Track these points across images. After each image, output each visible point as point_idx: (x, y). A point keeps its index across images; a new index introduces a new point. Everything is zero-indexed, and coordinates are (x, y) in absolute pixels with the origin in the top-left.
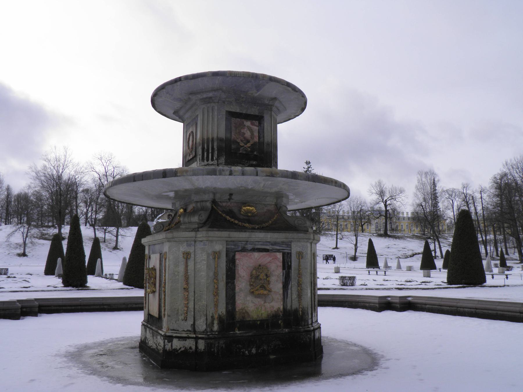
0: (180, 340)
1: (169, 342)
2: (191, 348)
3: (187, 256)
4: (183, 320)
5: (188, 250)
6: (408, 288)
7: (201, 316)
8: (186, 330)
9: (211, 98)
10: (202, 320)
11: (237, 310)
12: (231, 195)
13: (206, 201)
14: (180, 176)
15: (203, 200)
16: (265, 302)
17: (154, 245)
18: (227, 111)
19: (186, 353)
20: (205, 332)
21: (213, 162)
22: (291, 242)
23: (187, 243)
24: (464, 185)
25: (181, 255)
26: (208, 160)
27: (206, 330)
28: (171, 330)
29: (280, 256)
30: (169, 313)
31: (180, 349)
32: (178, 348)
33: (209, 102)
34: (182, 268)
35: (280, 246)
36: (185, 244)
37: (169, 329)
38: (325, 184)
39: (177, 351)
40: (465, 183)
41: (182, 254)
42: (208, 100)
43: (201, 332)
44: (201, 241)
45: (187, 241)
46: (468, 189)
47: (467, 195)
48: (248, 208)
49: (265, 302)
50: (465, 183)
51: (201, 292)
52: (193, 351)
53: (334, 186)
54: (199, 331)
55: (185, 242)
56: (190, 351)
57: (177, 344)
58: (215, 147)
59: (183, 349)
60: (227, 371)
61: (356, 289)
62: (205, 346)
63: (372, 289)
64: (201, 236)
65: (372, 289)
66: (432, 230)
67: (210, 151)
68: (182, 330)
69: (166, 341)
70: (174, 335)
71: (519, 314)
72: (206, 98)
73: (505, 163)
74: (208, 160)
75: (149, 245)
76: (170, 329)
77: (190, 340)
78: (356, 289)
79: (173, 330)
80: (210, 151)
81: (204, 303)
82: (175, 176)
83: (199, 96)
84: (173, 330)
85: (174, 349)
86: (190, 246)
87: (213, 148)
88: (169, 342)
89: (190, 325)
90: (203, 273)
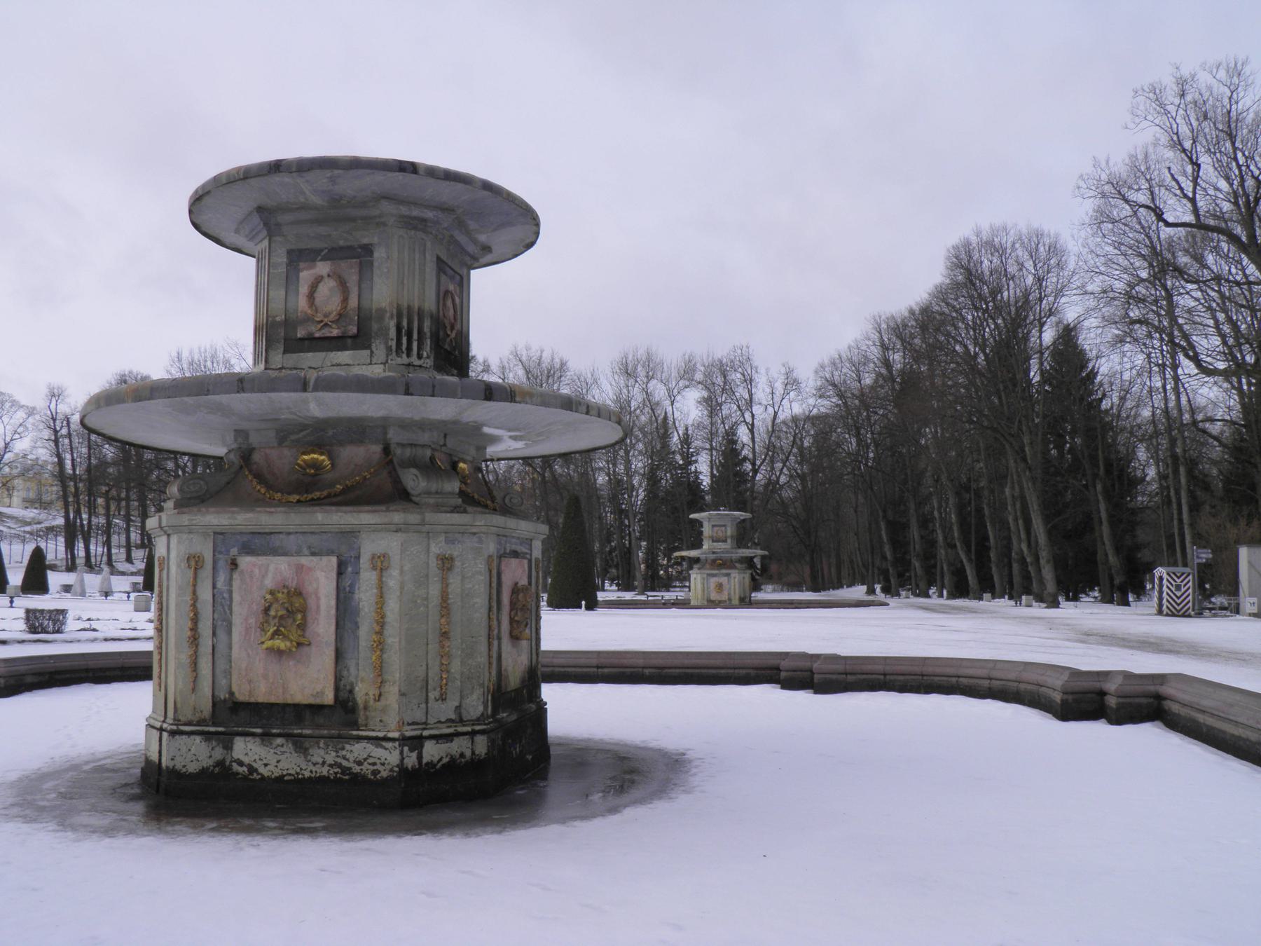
0: (440, 741)
1: (411, 750)
2: (462, 755)
3: (446, 563)
4: (437, 700)
5: (449, 552)
7: (473, 688)
8: (443, 720)
9: (424, 220)
10: (475, 696)
13: (423, 446)
14: (520, 403)
15: (415, 443)
17: (289, 534)
19: (453, 767)
20: (482, 718)
21: (422, 360)
22: (531, 540)
23: (446, 537)
24: (54, 388)
25: (433, 563)
26: (409, 355)
27: (482, 714)
28: (409, 724)
30: (402, 689)
31: (441, 759)
32: (435, 760)
33: (415, 228)
34: (434, 590)
36: (442, 538)
37: (403, 723)
39: (435, 765)
40: (55, 386)
41: (435, 560)
42: (414, 224)
43: (472, 720)
44: (474, 534)
45: (446, 533)
46: (63, 400)
47: (56, 413)
48: (315, 456)
50: (55, 386)
51: (474, 639)
52: (467, 762)
54: (469, 718)
55: (443, 535)
56: (461, 762)
57: (432, 751)
58: (426, 329)
59: (445, 760)
60: (319, 821)
61: (79, 641)
62: (488, 746)
63: (119, 640)
64: (482, 523)
65: (119, 640)
67: (415, 336)
68: (436, 721)
69: (406, 749)
70: (426, 733)
71: (595, 670)
72: (415, 218)
73: (174, 354)
74: (409, 355)
76: (406, 723)
77: (461, 738)
78: (79, 641)
79: (413, 723)
80: (415, 336)
81: (479, 660)
82: (511, 402)
83: (404, 210)
84: (413, 723)
85: (427, 764)
86: (454, 544)
87: (420, 331)
88: (411, 750)
89: (453, 709)
90: (478, 600)
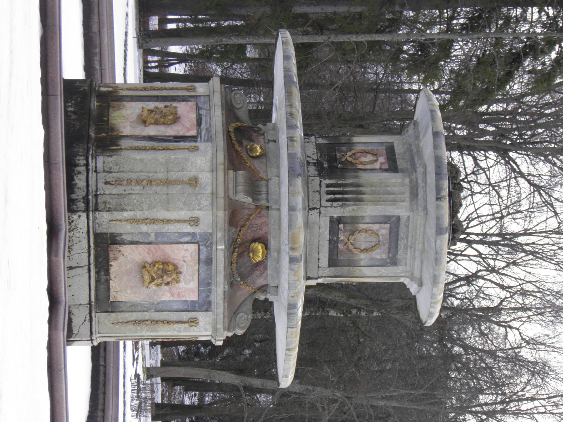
6: (108, 352)
11: (123, 103)
12: (275, 141)
16: (131, 122)
18: (393, 143)
29: (193, 133)
35: (205, 135)
38: (285, 93)
49: (131, 122)
53: (286, 111)
66: (235, 12)
74: (328, 193)
75: (209, 96)
